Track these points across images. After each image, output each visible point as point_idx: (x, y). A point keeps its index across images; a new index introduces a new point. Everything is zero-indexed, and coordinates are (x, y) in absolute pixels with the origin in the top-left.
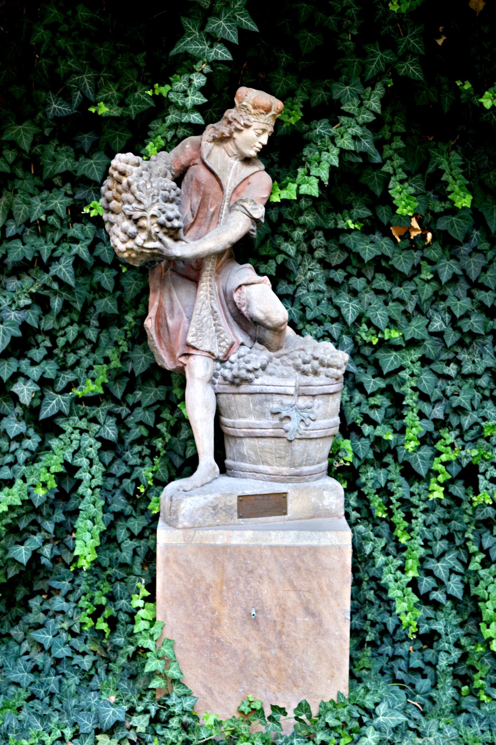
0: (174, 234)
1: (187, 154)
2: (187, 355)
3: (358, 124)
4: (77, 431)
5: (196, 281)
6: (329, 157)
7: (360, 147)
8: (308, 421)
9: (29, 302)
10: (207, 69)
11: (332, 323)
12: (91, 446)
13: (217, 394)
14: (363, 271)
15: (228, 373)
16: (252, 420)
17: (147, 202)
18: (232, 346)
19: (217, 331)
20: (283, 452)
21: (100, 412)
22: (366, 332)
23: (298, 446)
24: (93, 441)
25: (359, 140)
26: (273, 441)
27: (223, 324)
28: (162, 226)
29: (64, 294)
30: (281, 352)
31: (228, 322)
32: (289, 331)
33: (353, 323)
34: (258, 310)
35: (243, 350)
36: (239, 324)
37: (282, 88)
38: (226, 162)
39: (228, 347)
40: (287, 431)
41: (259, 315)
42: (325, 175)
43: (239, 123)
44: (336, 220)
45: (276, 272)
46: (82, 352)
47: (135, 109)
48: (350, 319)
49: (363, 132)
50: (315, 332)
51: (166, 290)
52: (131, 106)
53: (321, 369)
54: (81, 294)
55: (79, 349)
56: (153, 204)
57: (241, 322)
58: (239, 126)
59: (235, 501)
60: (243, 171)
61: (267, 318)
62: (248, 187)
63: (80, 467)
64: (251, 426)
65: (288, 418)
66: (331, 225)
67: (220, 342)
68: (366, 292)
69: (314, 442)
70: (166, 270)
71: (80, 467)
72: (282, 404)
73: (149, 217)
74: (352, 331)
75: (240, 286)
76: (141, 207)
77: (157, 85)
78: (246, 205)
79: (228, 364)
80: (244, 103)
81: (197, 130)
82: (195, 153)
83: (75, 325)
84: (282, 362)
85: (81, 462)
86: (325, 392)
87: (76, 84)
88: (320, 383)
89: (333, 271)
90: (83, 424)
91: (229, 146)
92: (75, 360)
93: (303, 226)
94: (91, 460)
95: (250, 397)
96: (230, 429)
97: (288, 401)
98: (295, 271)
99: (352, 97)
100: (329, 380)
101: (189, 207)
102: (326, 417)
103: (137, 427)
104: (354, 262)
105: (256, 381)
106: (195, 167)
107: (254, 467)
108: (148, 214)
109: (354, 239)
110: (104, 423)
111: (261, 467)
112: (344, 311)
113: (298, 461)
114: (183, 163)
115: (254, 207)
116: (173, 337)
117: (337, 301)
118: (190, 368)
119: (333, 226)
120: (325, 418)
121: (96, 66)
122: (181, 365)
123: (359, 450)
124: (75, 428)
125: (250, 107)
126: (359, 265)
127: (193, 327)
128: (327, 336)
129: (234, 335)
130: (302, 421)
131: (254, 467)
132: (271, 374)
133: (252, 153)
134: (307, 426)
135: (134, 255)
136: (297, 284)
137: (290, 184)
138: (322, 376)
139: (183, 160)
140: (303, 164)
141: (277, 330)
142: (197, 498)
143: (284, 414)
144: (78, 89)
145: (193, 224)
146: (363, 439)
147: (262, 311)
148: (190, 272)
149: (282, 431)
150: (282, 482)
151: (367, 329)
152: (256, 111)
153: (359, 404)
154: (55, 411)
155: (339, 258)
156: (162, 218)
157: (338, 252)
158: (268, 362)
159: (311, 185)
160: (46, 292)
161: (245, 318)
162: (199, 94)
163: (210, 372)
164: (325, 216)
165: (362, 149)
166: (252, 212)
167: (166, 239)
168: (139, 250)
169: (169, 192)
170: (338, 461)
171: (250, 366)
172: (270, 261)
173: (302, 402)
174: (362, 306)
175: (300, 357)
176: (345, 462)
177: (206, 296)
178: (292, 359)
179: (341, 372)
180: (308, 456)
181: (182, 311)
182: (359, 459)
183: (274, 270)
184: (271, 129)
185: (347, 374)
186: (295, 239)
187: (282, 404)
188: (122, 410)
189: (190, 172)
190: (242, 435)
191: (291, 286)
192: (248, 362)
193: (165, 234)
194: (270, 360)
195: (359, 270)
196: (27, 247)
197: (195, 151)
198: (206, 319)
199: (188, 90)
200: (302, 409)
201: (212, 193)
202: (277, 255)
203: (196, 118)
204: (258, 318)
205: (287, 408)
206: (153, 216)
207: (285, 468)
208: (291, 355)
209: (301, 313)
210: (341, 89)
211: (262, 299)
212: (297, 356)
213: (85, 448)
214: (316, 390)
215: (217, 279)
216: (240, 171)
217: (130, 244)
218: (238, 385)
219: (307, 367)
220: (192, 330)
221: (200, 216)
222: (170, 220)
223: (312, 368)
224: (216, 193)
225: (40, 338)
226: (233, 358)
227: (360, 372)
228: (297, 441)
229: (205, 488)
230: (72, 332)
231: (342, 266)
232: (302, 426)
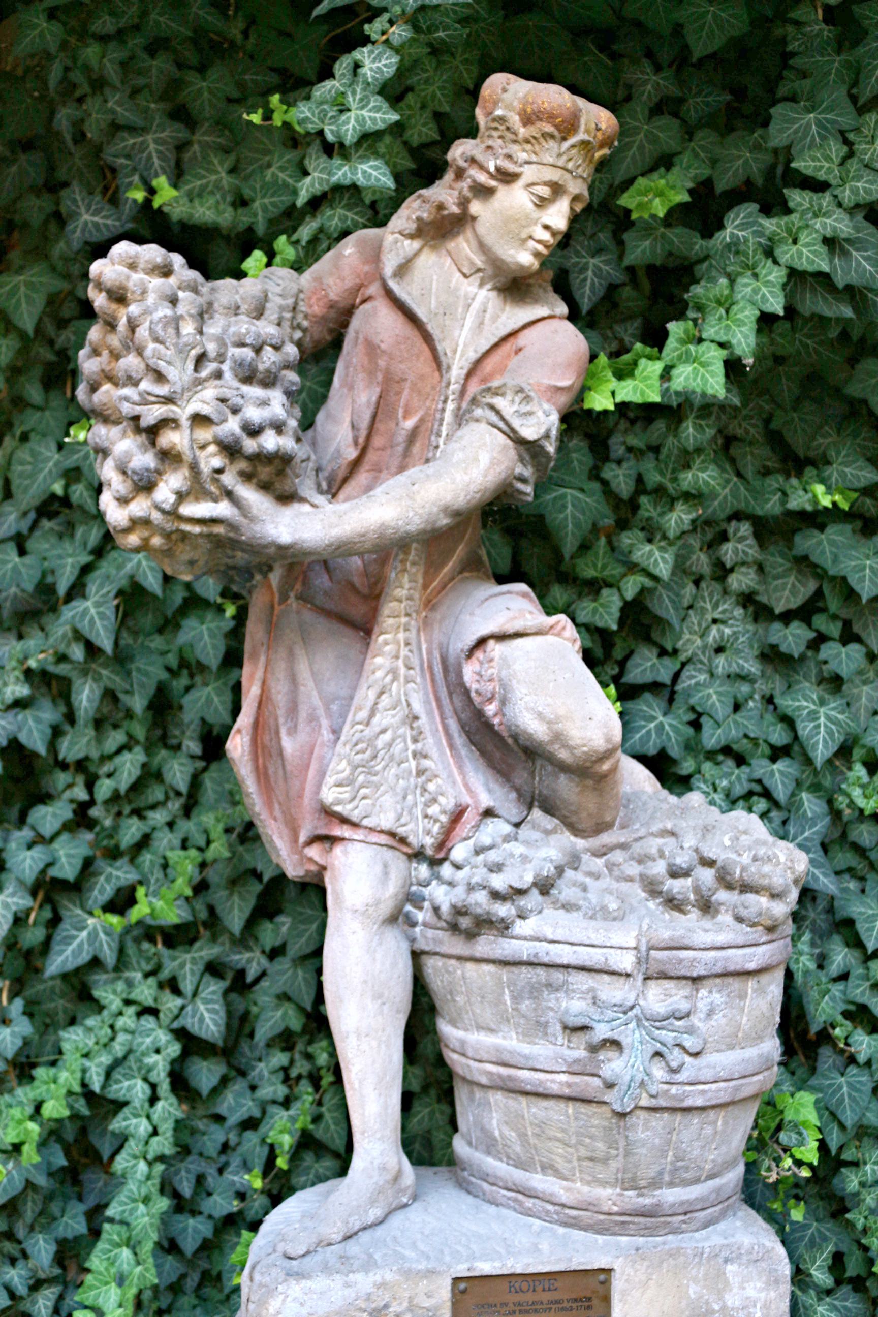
0: (275, 476)
1: (346, 272)
2: (331, 840)
3: (840, 205)
4: (131, 1010)
5: (365, 629)
6: (756, 291)
7: (847, 272)
8: (675, 1057)
9: (23, 691)
10: (400, 33)
11: (774, 759)
12: (158, 1051)
13: (416, 956)
14: (856, 628)
15: (440, 894)
16: (509, 1041)
17: (179, 373)
18: (457, 816)
19: (420, 772)
20: (600, 1145)
21: (186, 964)
22: (863, 786)
23: (647, 1132)
24: (163, 1037)
25: (845, 253)
26: (571, 1108)
27: (434, 753)
28: (230, 449)
29: (104, 672)
30: (606, 838)
31: (452, 746)
32: (637, 778)
33: (829, 762)
34: (529, 715)
35: (496, 828)
36: (483, 753)
37: (641, 147)
38: (453, 292)
39: (444, 819)
40: (610, 1086)
41: (536, 728)
42: (745, 341)
43: (482, 168)
44: (785, 494)
45: (621, 622)
46: (158, 817)
47: (265, 209)
48: (821, 751)
49: (857, 229)
50: (725, 783)
51: (282, 652)
52: (257, 205)
53: (722, 895)
54: (147, 674)
55: (153, 807)
56: (198, 382)
57: (490, 747)
58: (482, 178)
59: (445, 1293)
60: (504, 317)
61: (558, 737)
62: (515, 361)
63: (126, 1104)
64: (506, 1058)
65: (615, 1044)
66: (771, 506)
67: (427, 805)
68: (865, 682)
69: (695, 1120)
70: (284, 598)
71: (126, 1104)
72: (595, 1001)
73: (185, 423)
74: (827, 782)
75: (481, 642)
76: (163, 390)
77: (275, 99)
78: (500, 402)
79: (446, 870)
80: (499, 112)
81: (378, 213)
82: (366, 268)
83: (138, 749)
84: (610, 866)
85: (130, 1089)
86: (732, 968)
87: (128, 157)
88: (712, 937)
89: (777, 625)
90: (146, 992)
91: (463, 245)
92: (138, 836)
93: (692, 497)
94: (154, 1087)
95: (505, 974)
96: (455, 1056)
97: (614, 992)
98: (675, 622)
99: (823, 138)
100: (744, 933)
101: (347, 420)
102: (738, 1039)
103: (277, 1007)
104: (834, 604)
105: (521, 927)
106: (367, 306)
107: (518, 1175)
108: (183, 412)
109: (832, 543)
110: (195, 994)
111: (539, 1181)
112: (804, 729)
113: (647, 1172)
114: (333, 296)
115: (525, 408)
116: (295, 784)
117: (786, 703)
118: (334, 878)
119: (778, 510)
120: (731, 1047)
121: (181, 114)
122: (313, 868)
123: (841, 1101)
124: (128, 1002)
125: (515, 120)
126: (845, 613)
127: (359, 758)
128: (757, 795)
129: (466, 785)
130: (658, 1054)
131: (518, 1175)
132: (568, 907)
133: (525, 258)
134: (674, 1071)
135: (156, 541)
136: (683, 657)
137: (643, 362)
138: (725, 918)
139: (336, 289)
140: (680, 315)
141: (591, 772)
142: (319, 1283)
143: (602, 1031)
144: (135, 169)
145: (356, 464)
146: (852, 1070)
147: (540, 716)
148: (344, 596)
149: (596, 1082)
150: (599, 1232)
151: (865, 779)
152: (532, 131)
153: (844, 977)
154: (85, 957)
155: (794, 592)
156: (232, 426)
157: (792, 579)
158: (560, 871)
159: (703, 365)
160: (63, 669)
161: (496, 734)
162: (376, 101)
163: (392, 888)
164: (756, 483)
165: (853, 278)
166: (516, 423)
167: (249, 494)
168: (169, 526)
169: (258, 350)
170: (778, 1160)
171: (499, 882)
172: (605, 592)
173: (658, 998)
174: (855, 718)
175: (662, 855)
176: (799, 1163)
177: (394, 672)
178: (640, 862)
179: (781, 909)
180: (677, 1159)
181: (321, 712)
182: (842, 1127)
183: (617, 615)
184: (576, 187)
185: (807, 894)
186: (671, 534)
187: (595, 1001)
188: (250, 961)
189: (355, 323)
190: (484, 1080)
191: (667, 661)
192: (496, 868)
193: (247, 477)
194: (574, 861)
195: (847, 624)
196: (27, 560)
197: (366, 262)
198: (387, 737)
199: (354, 101)
200: (659, 1021)
201: (411, 377)
202: (624, 575)
203: (372, 173)
204: (530, 737)
205: (610, 1014)
206: (199, 419)
207: (609, 1191)
208: (637, 848)
209: (690, 731)
210: (794, 121)
211: (546, 677)
212: (654, 851)
213: (144, 1054)
214: (703, 962)
215: (426, 624)
216: (495, 318)
217: (139, 507)
218: (471, 936)
219: (677, 886)
220: (339, 768)
221: (377, 441)
222: (253, 431)
223: (697, 889)
224: (422, 377)
225: (62, 778)
226: (459, 852)
227: (845, 890)
228: (642, 1114)
229: (353, 1248)
230: (129, 766)
231: (804, 613)
232: (659, 1072)
